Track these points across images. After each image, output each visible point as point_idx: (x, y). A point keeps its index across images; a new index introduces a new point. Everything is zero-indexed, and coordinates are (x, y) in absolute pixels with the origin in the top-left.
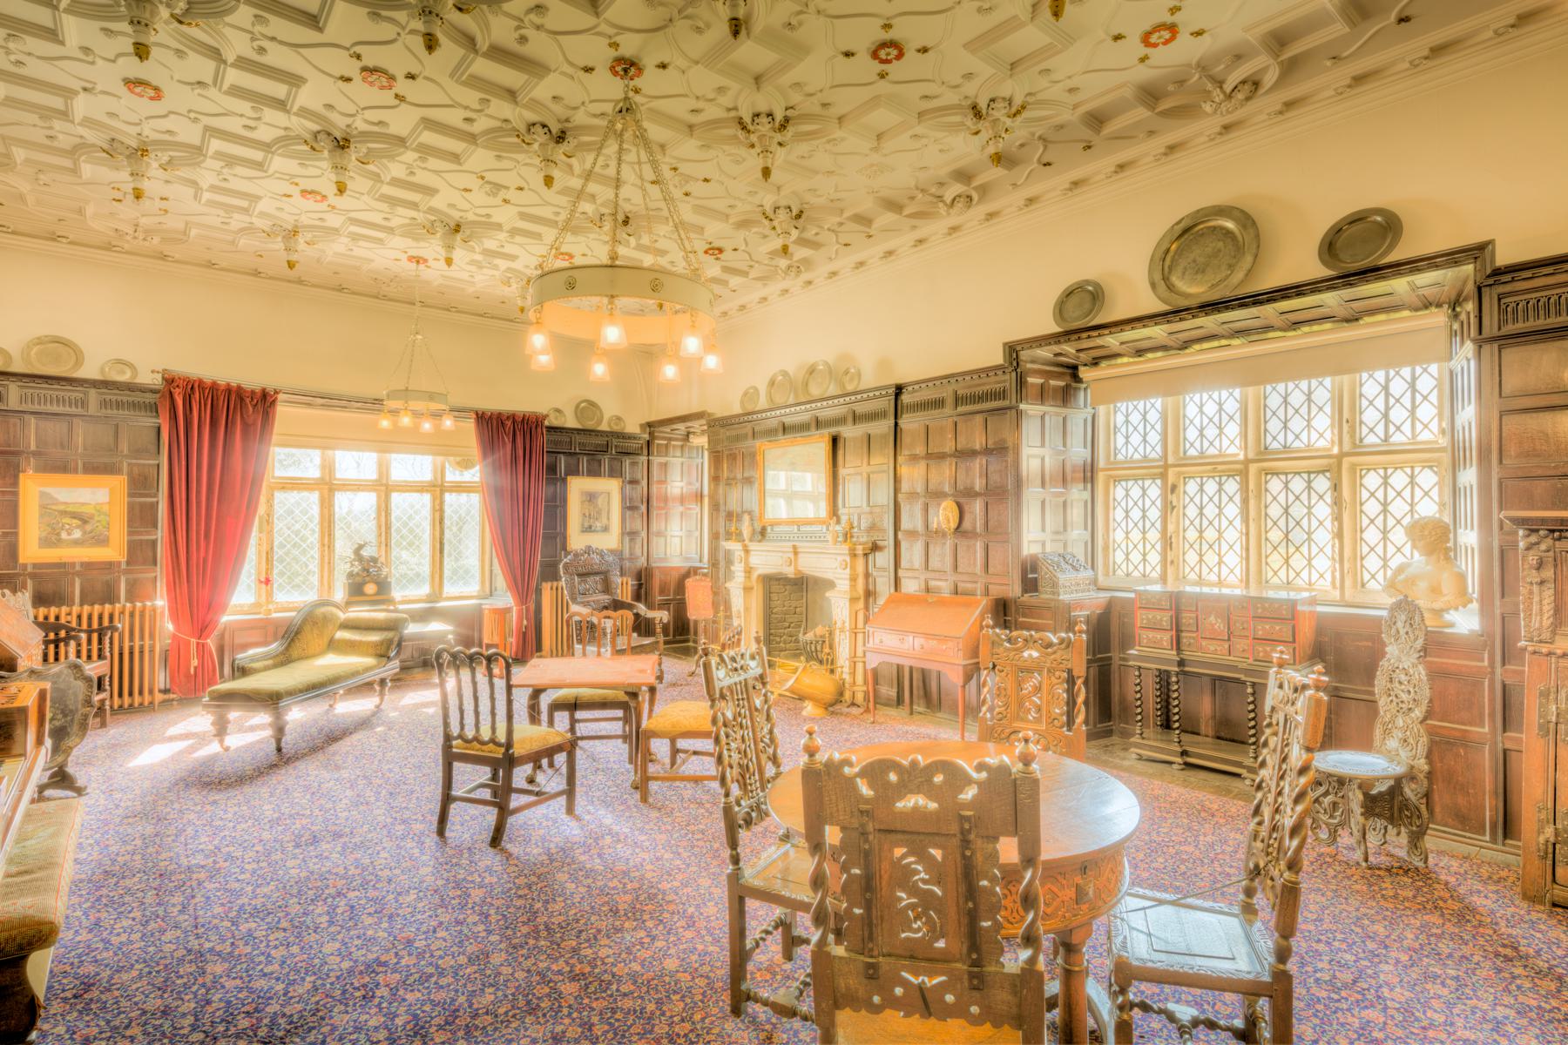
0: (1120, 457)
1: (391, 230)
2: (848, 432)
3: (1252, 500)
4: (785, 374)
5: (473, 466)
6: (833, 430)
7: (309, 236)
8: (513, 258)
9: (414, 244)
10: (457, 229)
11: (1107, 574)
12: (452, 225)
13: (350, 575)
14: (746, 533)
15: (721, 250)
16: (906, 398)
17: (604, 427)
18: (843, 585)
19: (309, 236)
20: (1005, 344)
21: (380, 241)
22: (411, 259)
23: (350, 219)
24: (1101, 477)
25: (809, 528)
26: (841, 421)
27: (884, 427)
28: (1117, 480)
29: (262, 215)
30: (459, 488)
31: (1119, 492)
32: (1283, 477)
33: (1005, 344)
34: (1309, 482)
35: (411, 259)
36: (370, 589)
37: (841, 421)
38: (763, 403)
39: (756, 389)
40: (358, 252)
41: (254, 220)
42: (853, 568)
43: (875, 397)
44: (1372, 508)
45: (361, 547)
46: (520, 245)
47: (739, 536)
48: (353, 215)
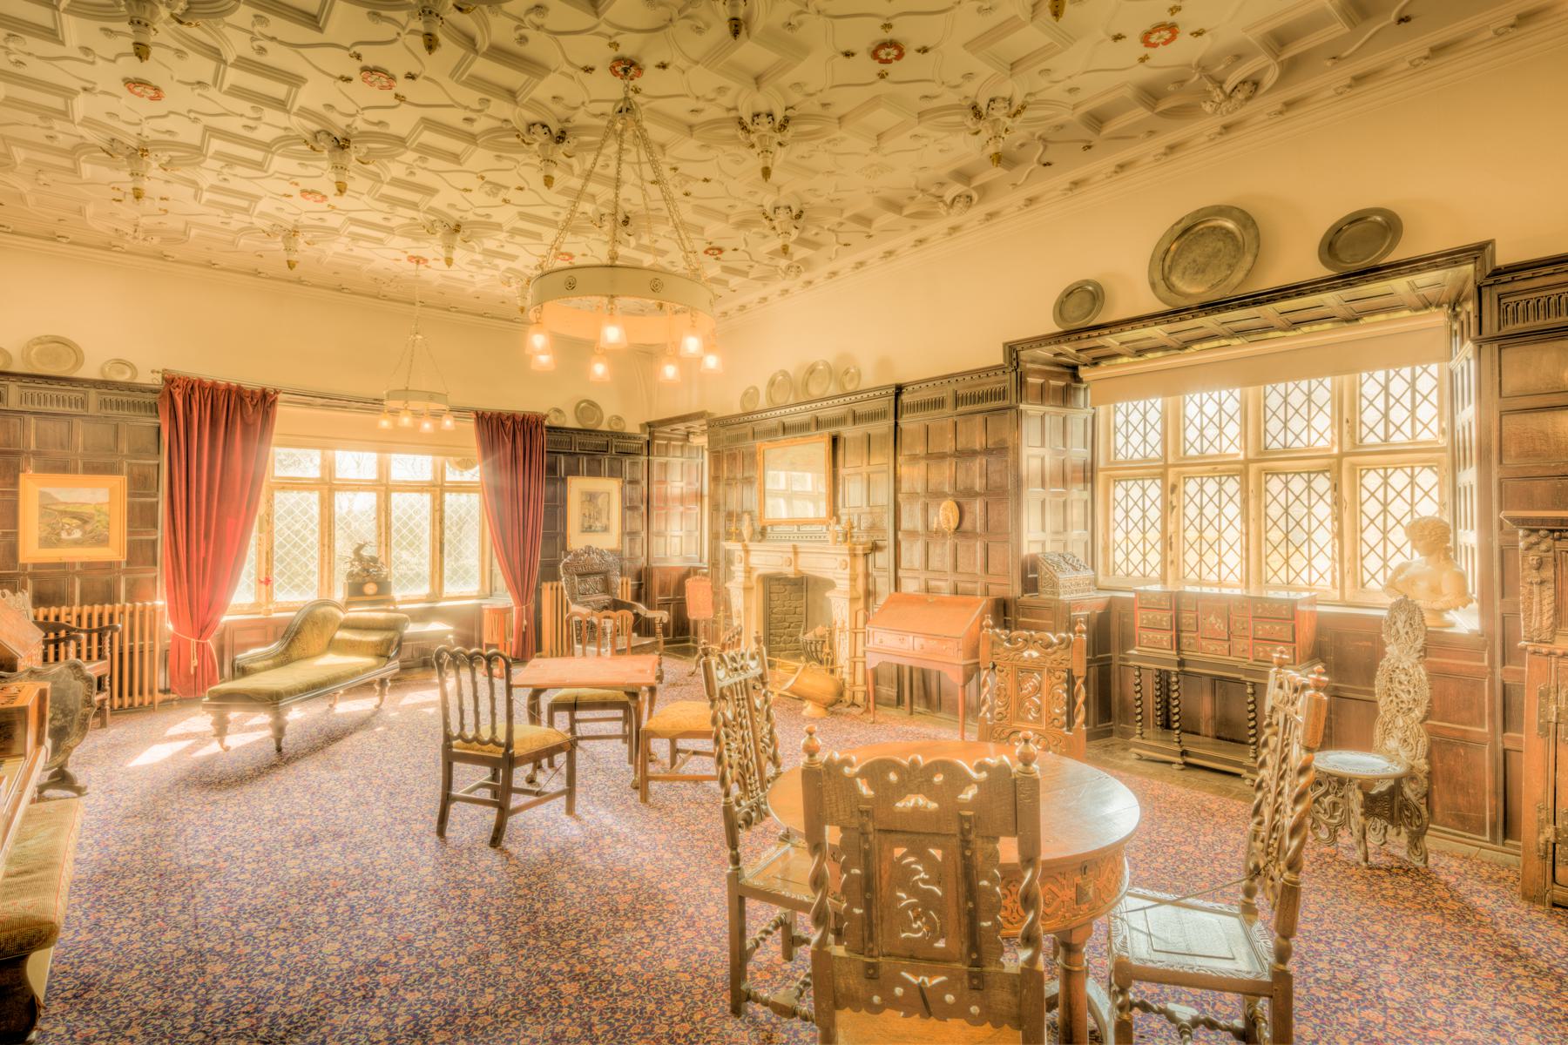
0: (1120, 457)
2: (848, 432)
4: (785, 374)
6: (833, 430)
8: (513, 258)
9: (415, 244)
10: (457, 228)
11: (1107, 574)
12: (452, 224)
13: (351, 575)
14: (746, 533)
15: (720, 250)
16: (906, 398)
17: (604, 427)
20: (1005, 344)
21: (380, 241)
22: (411, 258)
23: (350, 219)
25: (808, 528)
26: (841, 421)
27: (884, 427)
30: (459, 488)
31: (1119, 492)
33: (1005, 344)
34: (1309, 482)
35: (411, 258)
36: (370, 589)
37: (841, 421)
39: (756, 389)
40: (357, 252)
41: (254, 220)
42: (853, 568)
44: (1372, 508)
45: (361, 547)
46: (520, 245)
47: (739, 537)
48: (352, 215)
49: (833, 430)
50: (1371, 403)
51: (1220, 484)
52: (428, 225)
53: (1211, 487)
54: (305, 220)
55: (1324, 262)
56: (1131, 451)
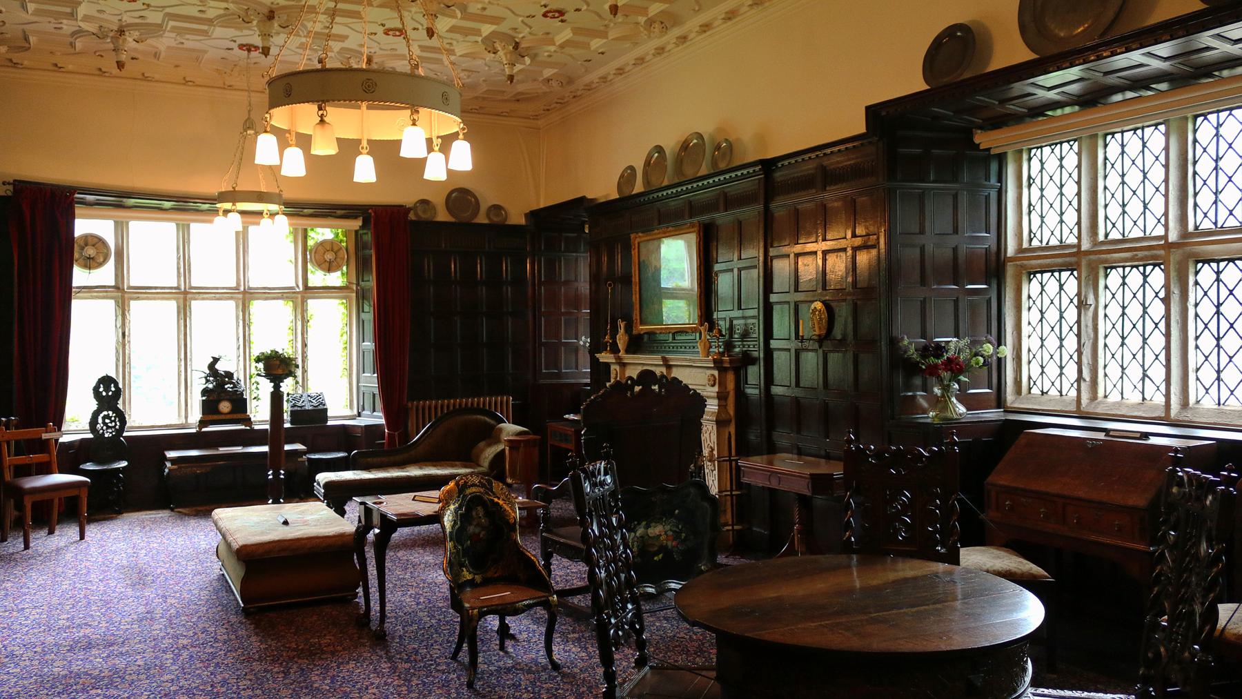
0: (1035, 243)
1: (210, 22)
2: (723, 218)
3: (1177, 291)
4: (700, 136)
5: (338, 268)
6: (705, 218)
7: (136, 34)
8: (343, 38)
9: (238, 33)
10: (271, 16)
11: (1018, 390)
12: (266, 11)
13: (205, 392)
14: (621, 345)
15: (561, 13)
16: (778, 175)
17: (482, 219)
18: (712, 406)
19: (136, 34)
20: (868, 108)
21: (205, 33)
22: (241, 47)
23: (168, 14)
24: (1010, 271)
25: (683, 337)
26: (711, 206)
27: (751, 213)
28: (1031, 274)
29: (86, 18)
30: (327, 291)
31: (1035, 286)
32: (1214, 265)
33: (868, 108)
34: (1218, 273)
35: (241, 47)
36: (225, 407)
37: (711, 206)
38: (639, 187)
39: (632, 168)
40: (189, 44)
41: (81, 24)
42: (722, 384)
43: (743, 177)
44: (1207, 310)
45: (216, 360)
46: (346, 25)
47: (615, 350)
48: (168, 10)
49: (705, 218)
50: (1157, 189)
51: (1145, 276)
52: (242, 14)
53: (1135, 278)
54: (127, 19)
55: (100, 265)
56: (1223, 213)
